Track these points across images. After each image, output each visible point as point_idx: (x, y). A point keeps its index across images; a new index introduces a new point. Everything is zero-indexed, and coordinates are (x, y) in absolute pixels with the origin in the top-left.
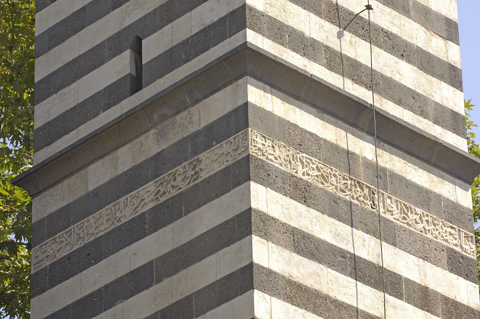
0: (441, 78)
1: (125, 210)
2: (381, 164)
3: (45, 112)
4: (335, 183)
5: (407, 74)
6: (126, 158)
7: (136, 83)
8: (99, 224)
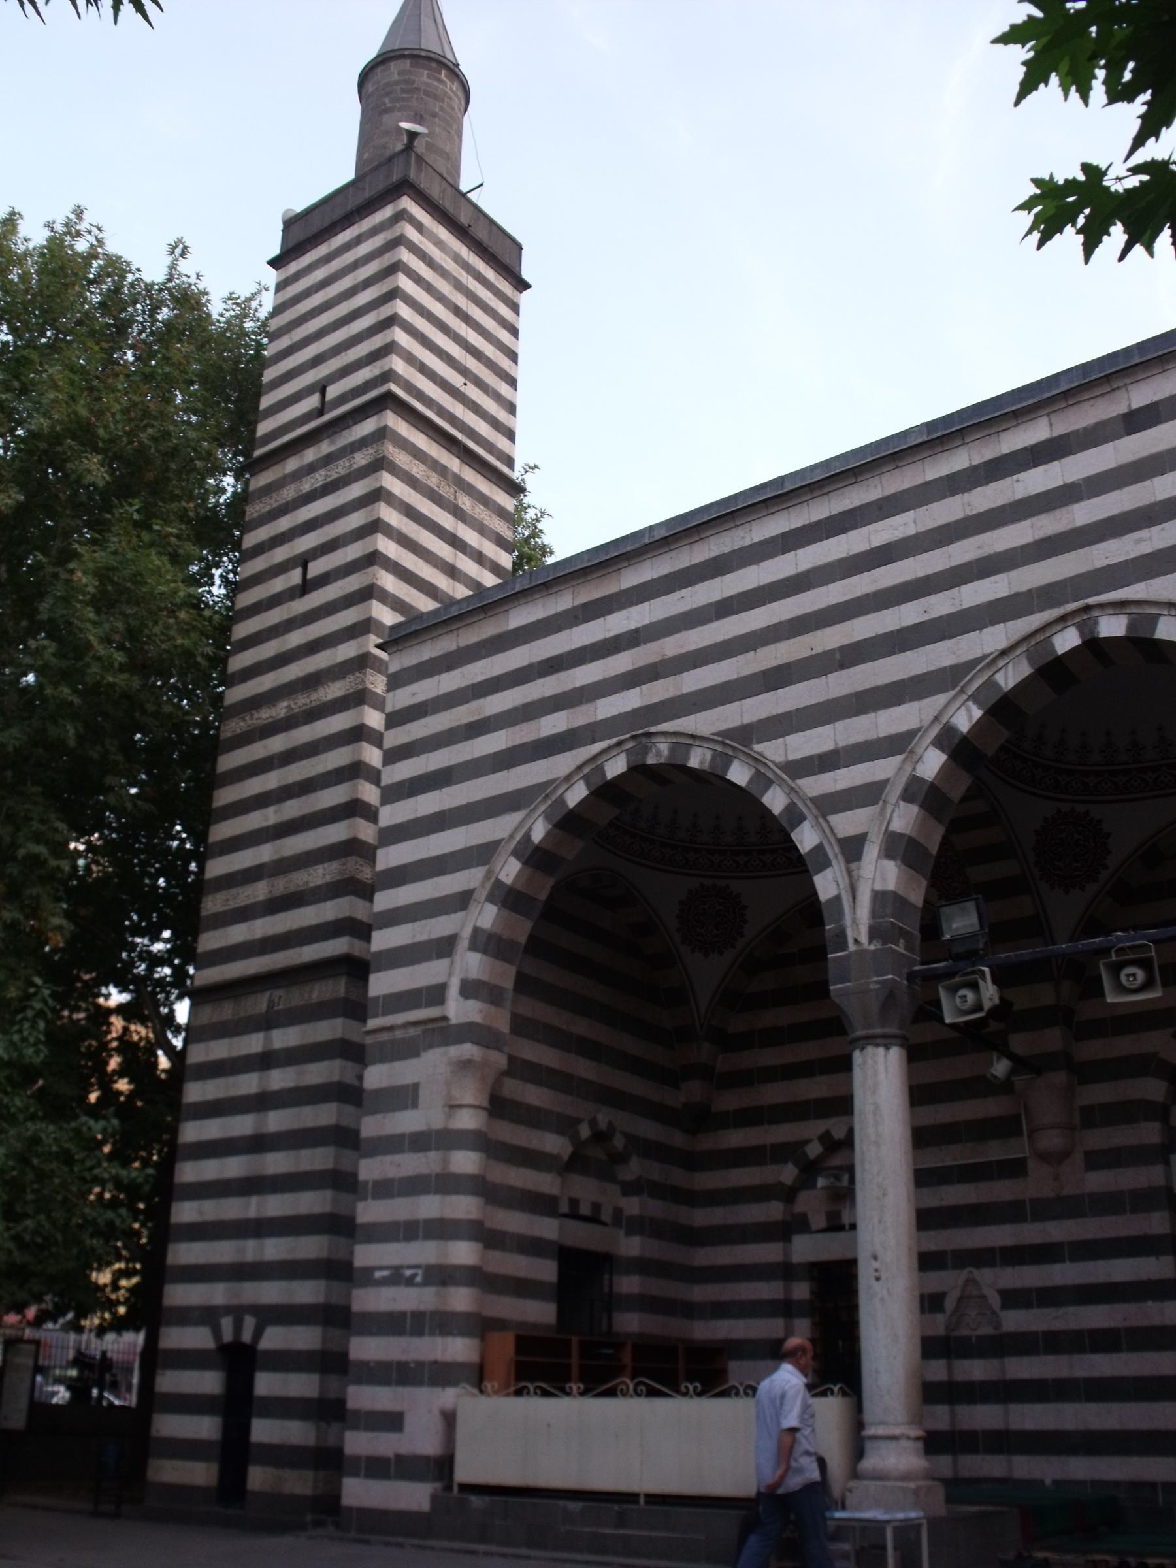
0: (503, 434)
1: (306, 486)
2: (463, 476)
3: (251, 539)
4: (433, 480)
5: (483, 428)
6: (310, 455)
7: (320, 412)
8: (288, 493)
